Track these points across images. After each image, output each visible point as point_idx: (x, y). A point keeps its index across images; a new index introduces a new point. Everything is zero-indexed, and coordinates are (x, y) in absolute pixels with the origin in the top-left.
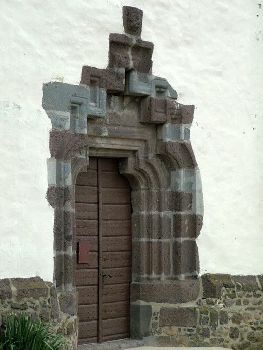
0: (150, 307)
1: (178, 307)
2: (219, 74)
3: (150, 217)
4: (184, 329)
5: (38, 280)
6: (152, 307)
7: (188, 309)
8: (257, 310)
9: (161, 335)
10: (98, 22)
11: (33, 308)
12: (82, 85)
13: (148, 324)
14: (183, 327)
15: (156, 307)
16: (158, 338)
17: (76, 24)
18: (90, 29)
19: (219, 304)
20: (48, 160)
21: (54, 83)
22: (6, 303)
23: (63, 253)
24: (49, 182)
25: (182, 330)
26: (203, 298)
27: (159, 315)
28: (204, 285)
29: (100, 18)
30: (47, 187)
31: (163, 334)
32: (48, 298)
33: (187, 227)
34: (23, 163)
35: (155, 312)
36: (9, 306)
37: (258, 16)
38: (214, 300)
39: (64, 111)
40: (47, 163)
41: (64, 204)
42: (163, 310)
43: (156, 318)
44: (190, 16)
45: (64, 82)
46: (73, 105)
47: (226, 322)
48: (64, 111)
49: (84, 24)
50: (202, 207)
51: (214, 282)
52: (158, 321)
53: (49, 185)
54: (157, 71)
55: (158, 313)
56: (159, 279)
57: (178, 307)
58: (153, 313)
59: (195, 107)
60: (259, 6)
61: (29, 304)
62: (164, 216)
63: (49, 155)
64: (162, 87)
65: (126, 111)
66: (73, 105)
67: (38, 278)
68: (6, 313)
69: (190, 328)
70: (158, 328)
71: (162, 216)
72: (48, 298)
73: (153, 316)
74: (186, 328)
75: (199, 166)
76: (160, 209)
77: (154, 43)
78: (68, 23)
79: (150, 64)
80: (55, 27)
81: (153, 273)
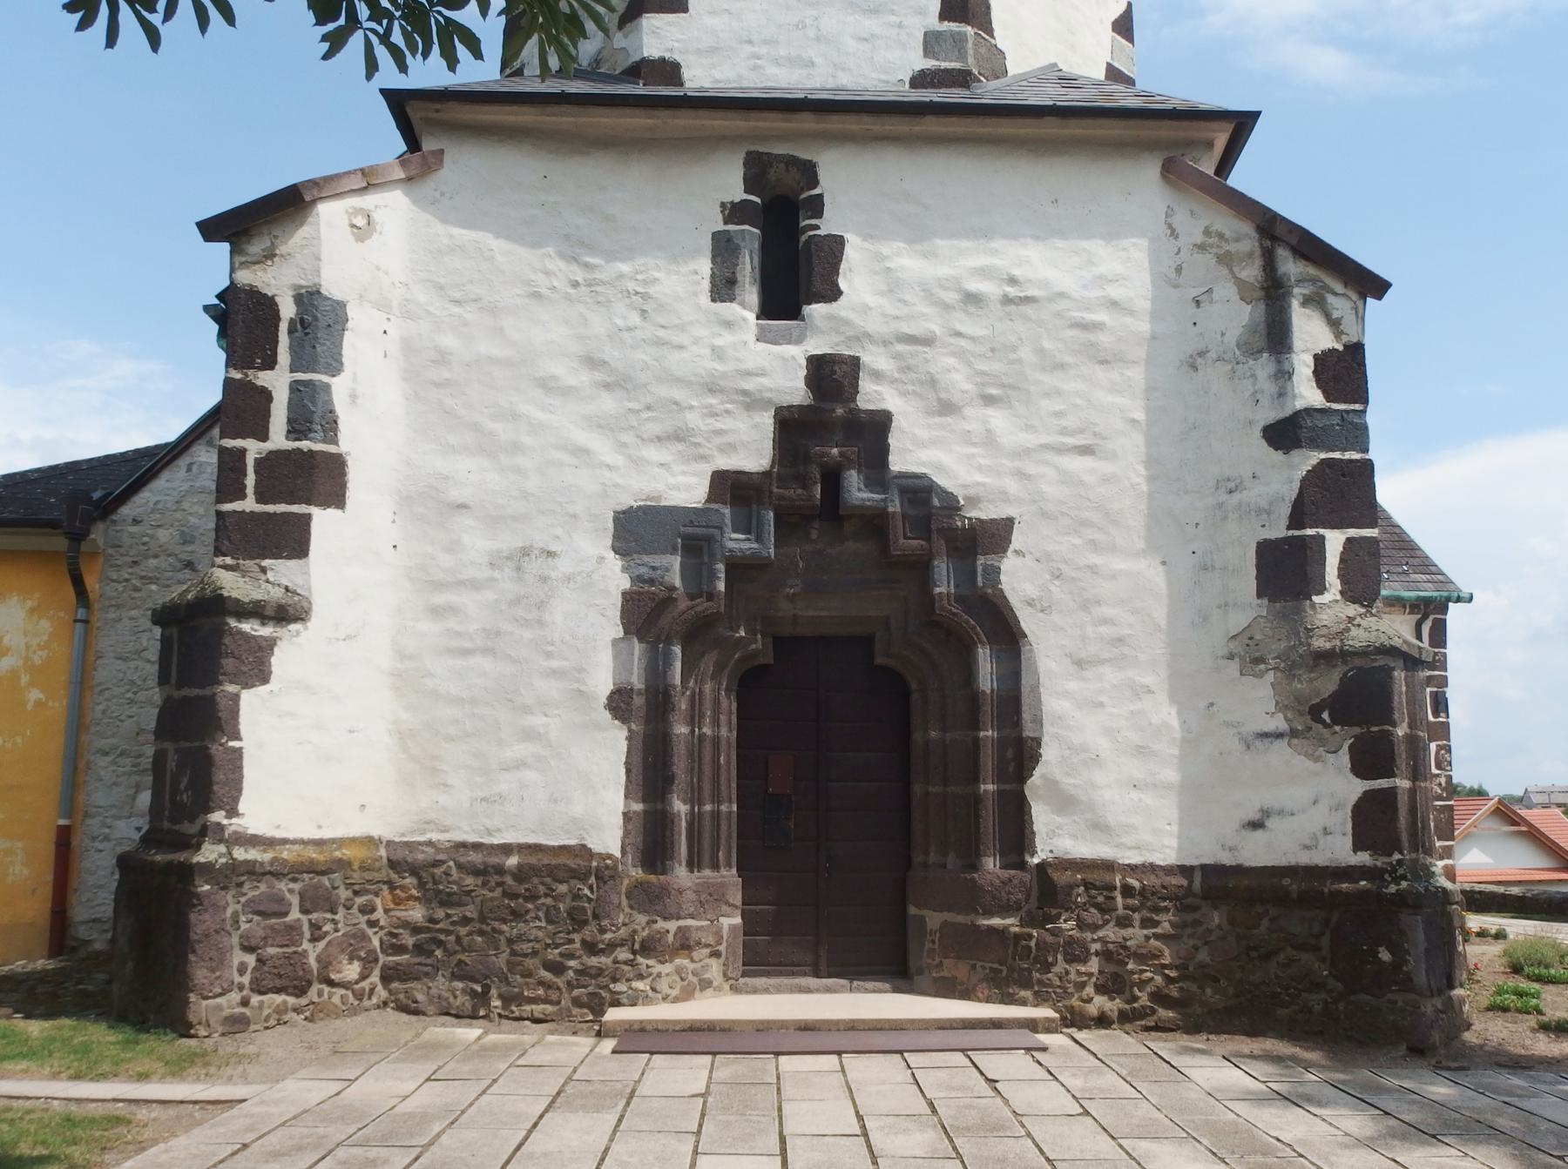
2: (1085, 450)
4: (983, 967)
5: (583, 851)
8: (1185, 939)
9: (942, 974)
10: (745, 393)
11: (552, 897)
12: (707, 506)
14: (981, 964)
15: (934, 920)
16: (936, 980)
17: (695, 403)
18: (729, 406)
21: (639, 507)
24: (614, 678)
25: (979, 969)
27: (938, 935)
29: (749, 385)
30: (611, 687)
31: (945, 974)
33: (1013, 764)
34: (550, 648)
35: (931, 930)
36: (499, 890)
37: (1195, 324)
38: (1054, 912)
40: (613, 645)
42: (945, 924)
43: (933, 942)
44: (993, 350)
45: (663, 503)
47: (1085, 961)
49: (712, 401)
50: (1038, 721)
52: (936, 946)
53: (614, 684)
54: (905, 457)
59: (1016, 522)
60: (1194, 305)
61: (542, 889)
63: (619, 632)
64: (919, 491)
67: (584, 846)
68: (492, 899)
70: (937, 960)
75: (1031, 637)
78: (676, 403)
79: (885, 450)
80: (645, 415)
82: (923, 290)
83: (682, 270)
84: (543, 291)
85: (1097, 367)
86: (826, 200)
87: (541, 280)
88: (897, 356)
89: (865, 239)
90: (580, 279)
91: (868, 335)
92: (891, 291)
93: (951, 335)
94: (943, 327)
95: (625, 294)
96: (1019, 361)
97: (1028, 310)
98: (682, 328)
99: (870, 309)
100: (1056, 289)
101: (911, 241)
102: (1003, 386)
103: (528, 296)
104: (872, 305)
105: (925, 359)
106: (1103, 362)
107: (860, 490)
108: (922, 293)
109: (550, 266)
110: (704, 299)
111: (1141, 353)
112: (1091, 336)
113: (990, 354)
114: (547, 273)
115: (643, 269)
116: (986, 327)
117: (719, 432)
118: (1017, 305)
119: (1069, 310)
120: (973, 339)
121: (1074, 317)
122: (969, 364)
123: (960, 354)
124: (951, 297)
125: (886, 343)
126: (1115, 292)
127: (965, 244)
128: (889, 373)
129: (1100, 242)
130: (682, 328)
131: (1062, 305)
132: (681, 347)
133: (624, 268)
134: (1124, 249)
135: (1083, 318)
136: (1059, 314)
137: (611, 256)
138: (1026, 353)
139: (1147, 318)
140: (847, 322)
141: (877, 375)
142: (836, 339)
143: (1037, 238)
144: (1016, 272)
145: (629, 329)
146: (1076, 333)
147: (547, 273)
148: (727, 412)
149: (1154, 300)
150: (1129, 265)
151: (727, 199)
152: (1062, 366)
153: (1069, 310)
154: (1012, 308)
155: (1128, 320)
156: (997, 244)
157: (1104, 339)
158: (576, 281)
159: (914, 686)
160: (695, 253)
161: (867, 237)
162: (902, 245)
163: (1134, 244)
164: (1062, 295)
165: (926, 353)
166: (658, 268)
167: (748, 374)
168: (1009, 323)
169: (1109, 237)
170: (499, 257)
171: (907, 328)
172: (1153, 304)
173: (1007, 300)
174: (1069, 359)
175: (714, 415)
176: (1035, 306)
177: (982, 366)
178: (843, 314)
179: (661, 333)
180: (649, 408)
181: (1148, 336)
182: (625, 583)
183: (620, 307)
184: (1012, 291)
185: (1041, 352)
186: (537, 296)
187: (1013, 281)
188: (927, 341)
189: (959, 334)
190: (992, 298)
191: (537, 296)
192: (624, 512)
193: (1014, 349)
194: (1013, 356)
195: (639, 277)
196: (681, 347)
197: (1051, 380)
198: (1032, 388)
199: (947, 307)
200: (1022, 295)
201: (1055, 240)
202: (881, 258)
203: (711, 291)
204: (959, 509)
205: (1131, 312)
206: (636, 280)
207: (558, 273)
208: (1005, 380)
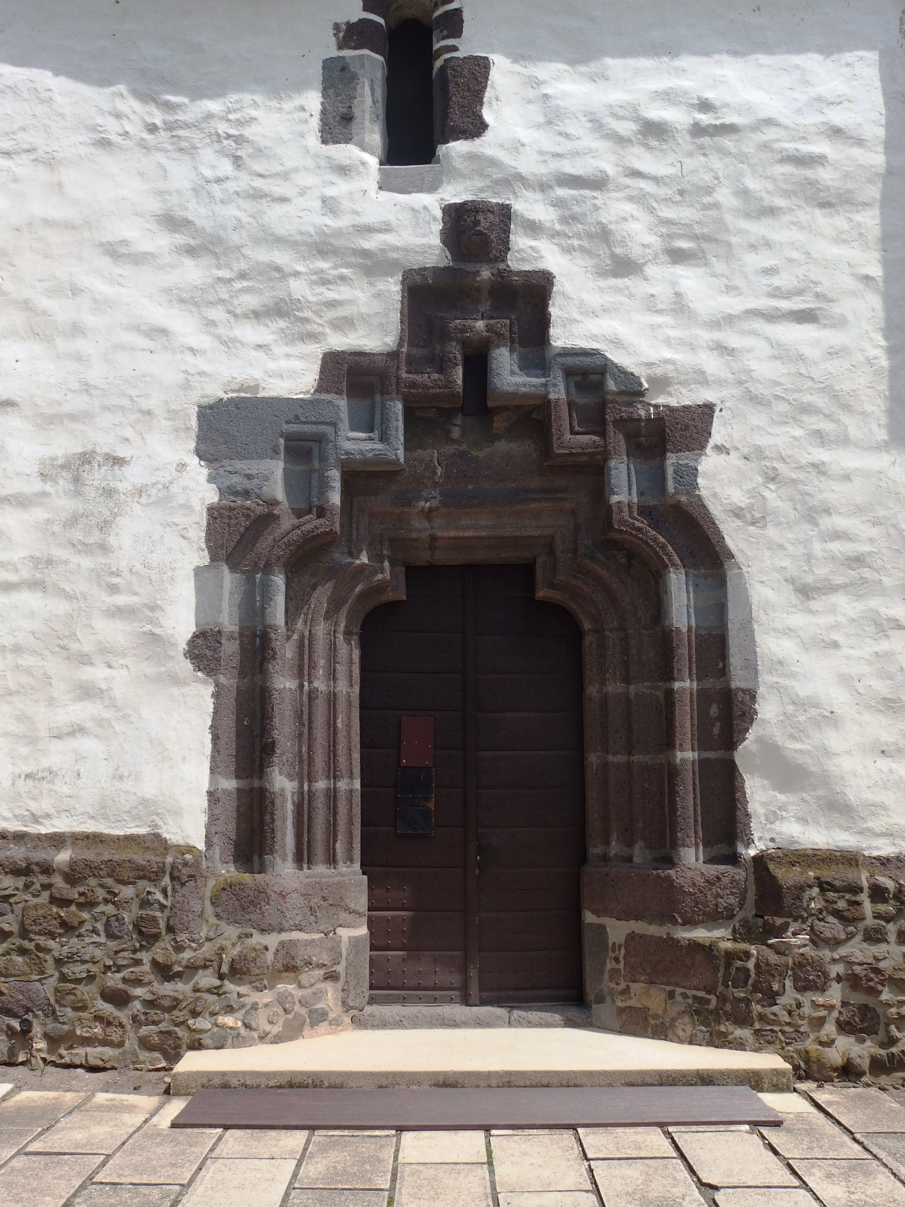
0: (602, 927)
1: (668, 934)
3: (605, 698)
4: (685, 996)
6: (608, 929)
7: (695, 946)
12: (317, 396)
13: (602, 971)
16: (621, 1011)
18: (345, 271)
19: (795, 934)
20: (198, 572)
21: (231, 400)
22: (37, 886)
23: (256, 783)
25: (679, 998)
26: (756, 916)
27: (623, 951)
28: (756, 879)
29: (370, 243)
30: (193, 629)
31: (633, 1003)
32: (163, 883)
33: (718, 724)
34: (115, 580)
35: (614, 944)
38: (779, 921)
39: (261, 457)
41: (261, 670)
42: (632, 937)
43: (617, 960)
46: (294, 443)
48: (262, 458)
50: (752, 667)
51: (786, 876)
52: (621, 966)
53: (197, 625)
55: (620, 946)
56: (630, 859)
57: (668, 934)
58: (610, 943)
62: (636, 695)
63: (203, 558)
65: (502, 446)
66: (294, 443)
69: (701, 994)
70: (622, 986)
71: (632, 697)
72: (163, 883)
73: (610, 954)
74: (690, 993)
76: (627, 680)
77: (553, 269)
78: (278, 269)
81: (614, 843)
82: (591, 121)
83: (284, 106)
84: (114, 138)
85: (818, 212)
86: (466, 16)
87: (112, 128)
88: (559, 203)
89: (515, 61)
90: (158, 122)
91: (520, 178)
92: (549, 122)
93: (626, 176)
94: (617, 165)
95: (215, 138)
96: (716, 206)
97: (727, 142)
98: (285, 176)
99: (523, 145)
100: (763, 115)
101: (572, 63)
102: (696, 238)
103: (93, 144)
104: (525, 140)
105: (595, 205)
106: (825, 205)
107: (513, 373)
108: (590, 125)
109: (121, 106)
110: (313, 140)
111: (874, 192)
112: (809, 173)
113: (678, 198)
114: (118, 116)
115: (236, 106)
116: (672, 164)
117: (332, 304)
118: (711, 135)
119: (778, 140)
120: (656, 179)
121: (785, 150)
122: (651, 211)
123: (639, 199)
124: (627, 128)
125: (543, 187)
126: (838, 117)
127: (643, 62)
128: (548, 225)
129: (817, 57)
130: (285, 176)
131: (770, 134)
132: (283, 200)
133: (213, 106)
134: (848, 65)
135: (797, 150)
136: (765, 147)
137: (197, 94)
138: (724, 196)
139: (881, 149)
140: (494, 163)
141: (534, 228)
142: (479, 183)
143: (735, 53)
144: (710, 95)
145: (219, 180)
146: (788, 169)
147: (118, 116)
148: (343, 278)
149: (888, 126)
150: (855, 83)
151: (342, 19)
152: (771, 212)
153: (778, 140)
154: (706, 140)
155: (856, 152)
156: (685, 61)
157: (825, 175)
158: (154, 124)
159: (587, 626)
160: (300, 86)
161: (517, 58)
162: (562, 66)
163: (861, 58)
164: (769, 122)
165: (595, 198)
166: (255, 105)
167: (368, 230)
168: (702, 158)
169: (827, 50)
170: (58, 99)
171: (569, 167)
172: (887, 130)
173: (698, 130)
174: (780, 202)
175: (325, 282)
176: (735, 137)
177: (668, 213)
178: (489, 152)
179: (259, 183)
180: (243, 276)
181: (882, 170)
182: (212, 496)
183: (207, 154)
184: (705, 119)
185: (744, 193)
186: (104, 144)
187: (705, 106)
188: (598, 183)
189: (636, 174)
190: (679, 128)
191: (104, 144)
192: (211, 407)
193: (709, 190)
194: (707, 200)
195: (232, 117)
196: (283, 200)
197: (757, 229)
198: (734, 240)
199: (621, 141)
200: (718, 122)
201: (759, 56)
202: (535, 83)
203: (322, 131)
204: (641, 394)
205: (860, 142)
206: (228, 120)
207: (131, 116)
208: (697, 230)
